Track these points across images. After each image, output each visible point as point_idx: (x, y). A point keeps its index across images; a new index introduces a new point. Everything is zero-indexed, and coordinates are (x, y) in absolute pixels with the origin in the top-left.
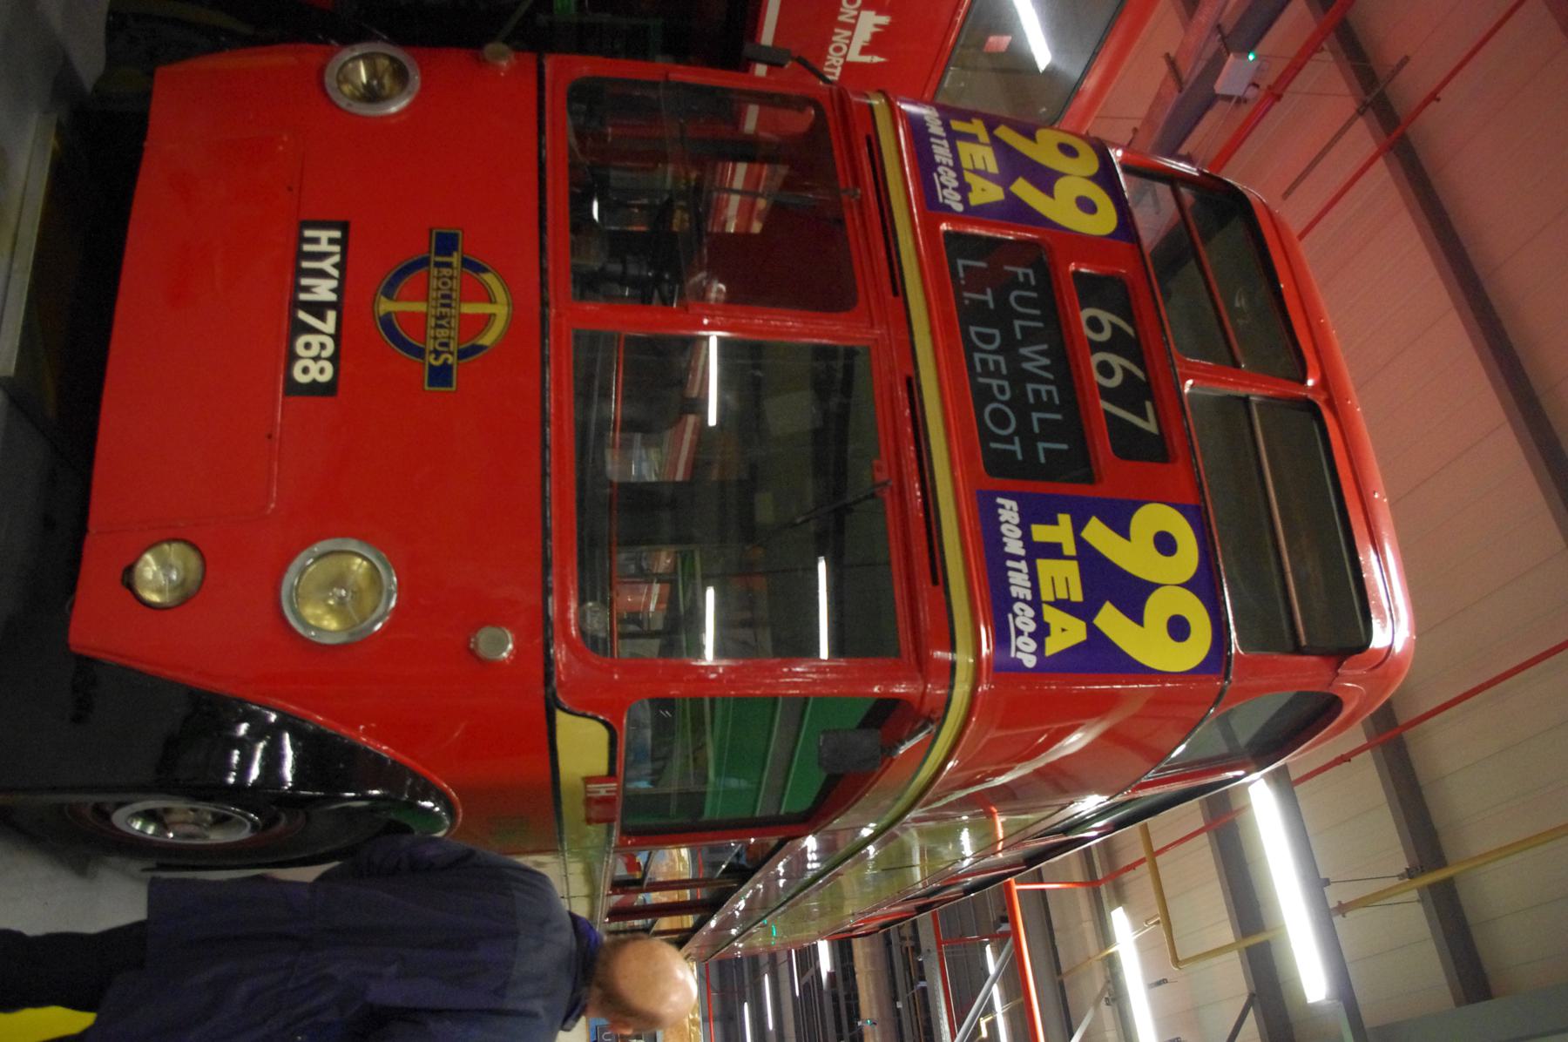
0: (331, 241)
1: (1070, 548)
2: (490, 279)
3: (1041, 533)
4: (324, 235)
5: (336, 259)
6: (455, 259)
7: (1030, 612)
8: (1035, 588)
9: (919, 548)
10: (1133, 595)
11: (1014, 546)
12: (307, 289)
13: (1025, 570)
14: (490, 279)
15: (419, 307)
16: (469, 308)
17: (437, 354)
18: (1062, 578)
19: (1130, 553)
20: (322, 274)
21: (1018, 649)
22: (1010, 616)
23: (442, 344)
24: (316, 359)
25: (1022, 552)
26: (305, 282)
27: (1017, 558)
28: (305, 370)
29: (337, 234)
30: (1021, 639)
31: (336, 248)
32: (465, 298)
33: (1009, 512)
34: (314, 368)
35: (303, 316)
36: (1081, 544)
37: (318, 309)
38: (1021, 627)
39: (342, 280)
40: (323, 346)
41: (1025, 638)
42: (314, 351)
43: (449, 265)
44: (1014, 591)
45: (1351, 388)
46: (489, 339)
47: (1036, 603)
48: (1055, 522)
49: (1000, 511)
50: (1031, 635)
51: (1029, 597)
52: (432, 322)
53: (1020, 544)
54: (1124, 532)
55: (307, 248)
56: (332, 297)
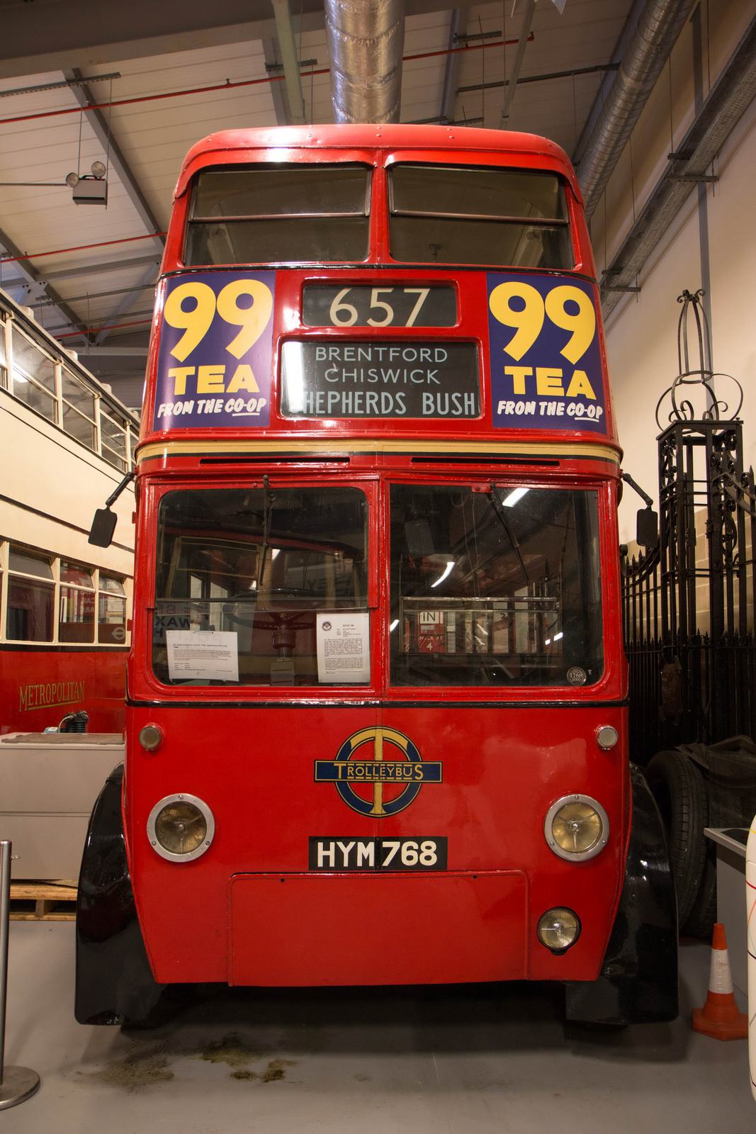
0: (326, 848)
1: (191, 370)
2: (355, 741)
3: (520, 388)
4: (321, 853)
5: (340, 844)
6: (340, 765)
7: (572, 405)
8: (215, 396)
9: (464, 468)
10: (220, 332)
11: (530, 408)
12: (366, 861)
13: (204, 401)
14: (355, 741)
15: (379, 788)
16: (379, 755)
17: (415, 774)
18: (548, 379)
19: (196, 328)
20: (353, 853)
21: (255, 411)
22: (234, 415)
23: (408, 772)
24: (419, 852)
25: (192, 402)
26: (360, 863)
27: (196, 406)
28: (428, 858)
29: (320, 845)
30: (248, 409)
31: (332, 845)
32: (372, 758)
33: (505, 407)
34: (426, 853)
35: (386, 863)
36: (187, 363)
37: (381, 853)
38: (580, 414)
39: (357, 839)
40: (410, 848)
41: (248, 406)
42: (414, 854)
43: (345, 769)
44: (218, 410)
45: (185, 158)
46: (403, 742)
47: (226, 397)
48: (511, 377)
49: (507, 413)
50: (246, 402)
51: (222, 401)
52: (390, 779)
53: (186, 403)
54: (181, 332)
55: (332, 864)
56: (371, 845)
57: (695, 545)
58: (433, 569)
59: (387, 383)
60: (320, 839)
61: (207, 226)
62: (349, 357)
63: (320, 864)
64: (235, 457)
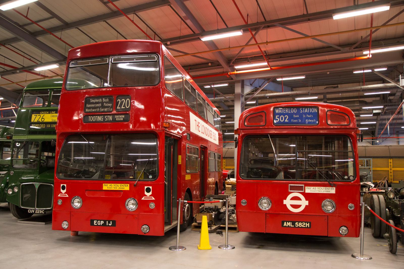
4: (308, 225)
29: (309, 227)
57: (138, 235)
58: (325, 158)
59: (151, 124)
60: (309, 228)
61: (176, 209)
62: (95, 223)
63: (309, 223)
64: (315, 134)
